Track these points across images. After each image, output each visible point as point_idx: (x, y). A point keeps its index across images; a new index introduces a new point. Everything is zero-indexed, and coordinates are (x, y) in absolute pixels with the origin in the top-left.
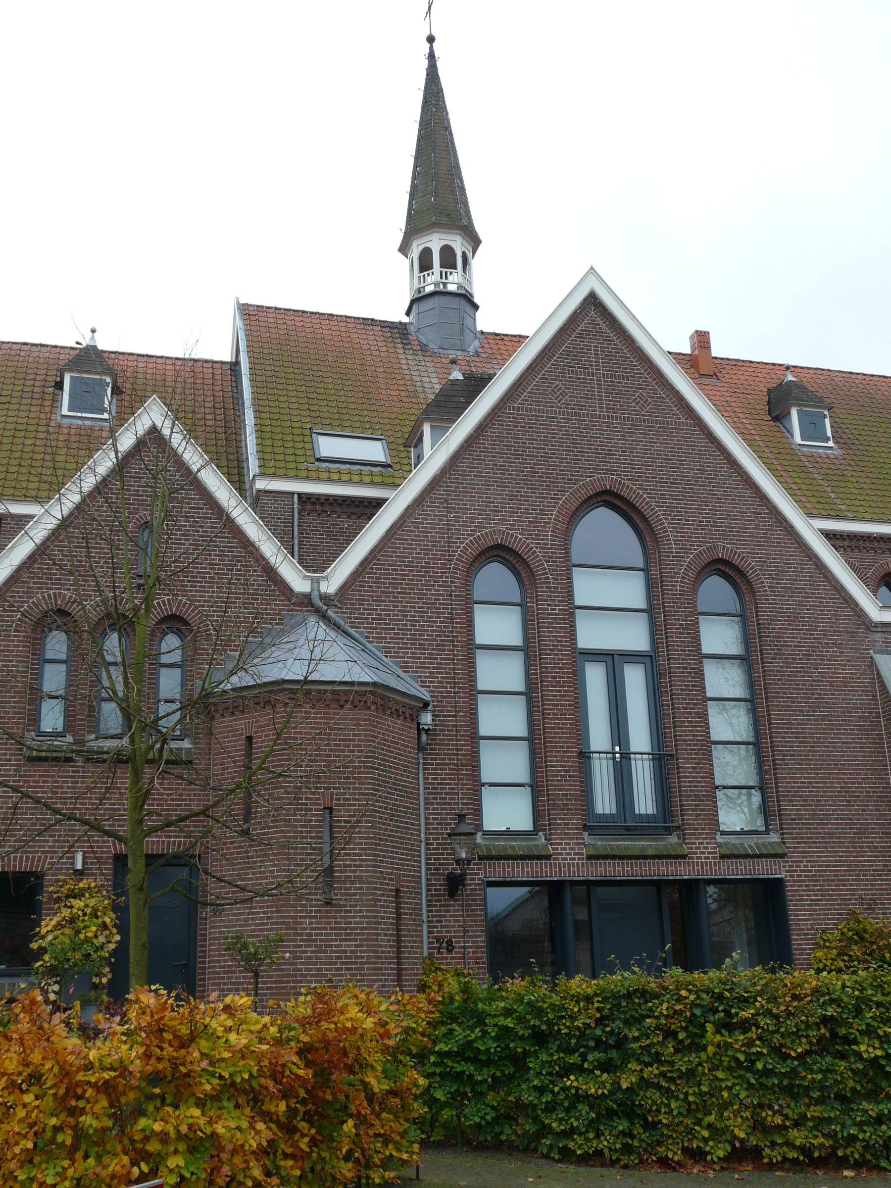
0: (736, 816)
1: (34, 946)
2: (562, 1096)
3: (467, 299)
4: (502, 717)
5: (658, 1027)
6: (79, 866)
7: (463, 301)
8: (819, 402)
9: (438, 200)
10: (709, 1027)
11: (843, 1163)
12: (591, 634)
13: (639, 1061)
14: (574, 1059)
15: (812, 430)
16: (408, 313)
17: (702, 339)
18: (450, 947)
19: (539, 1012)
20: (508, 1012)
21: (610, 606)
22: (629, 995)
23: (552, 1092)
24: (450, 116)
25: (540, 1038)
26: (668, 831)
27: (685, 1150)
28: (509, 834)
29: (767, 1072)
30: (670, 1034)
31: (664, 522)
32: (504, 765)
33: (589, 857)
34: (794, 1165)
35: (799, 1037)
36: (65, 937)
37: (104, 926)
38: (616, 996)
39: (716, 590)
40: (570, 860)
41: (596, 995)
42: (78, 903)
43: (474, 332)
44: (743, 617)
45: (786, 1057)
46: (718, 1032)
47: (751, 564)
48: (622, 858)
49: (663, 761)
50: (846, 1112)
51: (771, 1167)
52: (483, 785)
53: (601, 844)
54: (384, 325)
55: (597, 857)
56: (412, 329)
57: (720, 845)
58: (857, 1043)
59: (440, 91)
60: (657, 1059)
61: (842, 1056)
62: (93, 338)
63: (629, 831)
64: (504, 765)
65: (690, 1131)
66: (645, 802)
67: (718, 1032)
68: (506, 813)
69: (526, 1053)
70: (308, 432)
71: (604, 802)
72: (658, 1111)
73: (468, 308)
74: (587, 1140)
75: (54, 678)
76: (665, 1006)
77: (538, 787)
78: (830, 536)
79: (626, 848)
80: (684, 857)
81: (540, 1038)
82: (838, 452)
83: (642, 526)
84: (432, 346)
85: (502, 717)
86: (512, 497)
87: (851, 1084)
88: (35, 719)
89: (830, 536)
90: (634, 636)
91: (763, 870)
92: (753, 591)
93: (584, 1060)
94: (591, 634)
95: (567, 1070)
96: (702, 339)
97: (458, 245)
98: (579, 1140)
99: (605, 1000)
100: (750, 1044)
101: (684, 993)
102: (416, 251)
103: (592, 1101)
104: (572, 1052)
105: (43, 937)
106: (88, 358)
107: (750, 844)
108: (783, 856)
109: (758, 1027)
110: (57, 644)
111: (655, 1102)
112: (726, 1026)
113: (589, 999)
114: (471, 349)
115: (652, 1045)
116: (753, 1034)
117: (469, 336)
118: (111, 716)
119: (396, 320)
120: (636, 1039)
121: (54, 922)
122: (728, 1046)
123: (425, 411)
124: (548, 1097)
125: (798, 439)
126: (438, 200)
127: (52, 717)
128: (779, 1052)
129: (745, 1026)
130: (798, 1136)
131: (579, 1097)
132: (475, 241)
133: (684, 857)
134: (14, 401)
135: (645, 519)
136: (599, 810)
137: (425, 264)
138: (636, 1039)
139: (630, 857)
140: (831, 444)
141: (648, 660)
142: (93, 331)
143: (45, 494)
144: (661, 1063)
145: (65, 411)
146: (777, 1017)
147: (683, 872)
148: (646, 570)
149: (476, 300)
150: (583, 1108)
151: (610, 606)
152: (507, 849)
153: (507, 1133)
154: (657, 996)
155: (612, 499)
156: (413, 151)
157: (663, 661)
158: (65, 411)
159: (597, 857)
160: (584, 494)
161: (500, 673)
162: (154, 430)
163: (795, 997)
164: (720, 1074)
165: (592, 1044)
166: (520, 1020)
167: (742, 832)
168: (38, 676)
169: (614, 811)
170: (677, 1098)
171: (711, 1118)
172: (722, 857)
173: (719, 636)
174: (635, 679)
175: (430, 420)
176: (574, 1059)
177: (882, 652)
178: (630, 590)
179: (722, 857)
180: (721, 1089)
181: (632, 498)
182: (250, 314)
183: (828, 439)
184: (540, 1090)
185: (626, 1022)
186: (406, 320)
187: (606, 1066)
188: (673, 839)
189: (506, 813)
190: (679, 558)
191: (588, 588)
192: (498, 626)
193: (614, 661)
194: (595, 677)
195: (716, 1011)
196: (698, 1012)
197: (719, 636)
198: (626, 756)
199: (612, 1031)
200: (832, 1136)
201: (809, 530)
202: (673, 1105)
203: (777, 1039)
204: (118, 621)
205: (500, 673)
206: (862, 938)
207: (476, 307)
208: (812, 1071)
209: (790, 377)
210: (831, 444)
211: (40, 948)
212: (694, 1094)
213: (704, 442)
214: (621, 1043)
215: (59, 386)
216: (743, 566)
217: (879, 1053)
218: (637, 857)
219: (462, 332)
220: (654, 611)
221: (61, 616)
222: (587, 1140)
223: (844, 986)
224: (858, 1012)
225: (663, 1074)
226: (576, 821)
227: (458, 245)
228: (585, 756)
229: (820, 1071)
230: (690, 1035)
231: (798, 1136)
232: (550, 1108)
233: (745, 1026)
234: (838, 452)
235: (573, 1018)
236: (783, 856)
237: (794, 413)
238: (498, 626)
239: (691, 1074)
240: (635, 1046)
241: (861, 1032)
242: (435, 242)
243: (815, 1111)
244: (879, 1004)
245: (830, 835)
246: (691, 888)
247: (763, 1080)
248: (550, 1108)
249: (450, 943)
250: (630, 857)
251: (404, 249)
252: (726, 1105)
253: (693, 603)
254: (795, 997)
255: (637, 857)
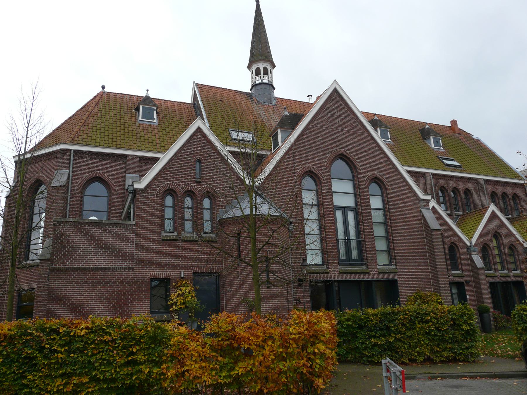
0: (382, 259)
1: (169, 303)
2: (370, 345)
3: (271, 86)
4: (312, 227)
5: (399, 323)
6: (182, 276)
7: (262, 85)
8: (386, 127)
9: (260, 52)
10: (416, 322)
11: (459, 361)
12: (338, 201)
13: (394, 333)
14: (373, 333)
15: (437, 143)
16: (251, 90)
17: (454, 122)
18: (300, 302)
19: (360, 319)
20: (348, 320)
21: (343, 193)
22: (389, 314)
23: (366, 344)
24: (265, 22)
25: (361, 327)
26: (362, 265)
27: (409, 359)
28: (315, 265)
29: (435, 335)
30: (403, 325)
31: (359, 165)
32: (312, 242)
33: (340, 273)
34: (442, 362)
35: (445, 324)
36: (180, 300)
37: (192, 296)
38: (385, 314)
39: (374, 188)
40: (335, 274)
41: (378, 314)
42: (183, 289)
43: (274, 97)
44: (382, 196)
45: (440, 331)
46: (419, 324)
47: (385, 179)
48: (350, 273)
49: (360, 243)
50: (459, 346)
51: (436, 363)
52: (307, 249)
53: (343, 269)
54: (244, 93)
55: (343, 273)
56: (253, 95)
57: (378, 269)
58: (462, 326)
59: (261, 13)
60: (400, 332)
61: (457, 330)
62: (147, 93)
63: (351, 265)
64: (312, 242)
65: (411, 354)
66: (355, 255)
67: (419, 324)
68: (314, 258)
69: (357, 332)
70: (227, 130)
71: (343, 256)
72: (401, 348)
73: (272, 90)
74: (378, 358)
75: (169, 213)
76: (401, 316)
77: (324, 251)
78: (409, 172)
79: (351, 270)
80: (368, 273)
81: (361, 327)
82: (392, 143)
83: (352, 166)
84: (261, 101)
85: (312, 227)
86: (313, 155)
87: (460, 338)
88: (163, 227)
89: (409, 172)
90: (349, 201)
91: (391, 277)
92: (386, 188)
93: (376, 333)
94: (338, 201)
95: (370, 338)
96: (454, 122)
97: (269, 67)
98: (376, 358)
99: (382, 315)
100: (429, 327)
101: (407, 312)
102: (254, 68)
103: (379, 346)
104: (371, 331)
105: (172, 300)
106: (147, 100)
107: (387, 268)
108: (396, 273)
109: (432, 322)
110: (169, 201)
111: (399, 346)
112: (422, 321)
113: (376, 315)
114: (274, 103)
115: (398, 328)
116: (430, 324)
117: (273, 99)
118: (188, 226)
119: (248, 92)
120: (393, 327)
121: (176, 295)
122: (423, 328)
123: (278, 125)
124: (364, 346)
125: (433, 146)
126: (260, 52)
127: (169, 225)
128: (438, 329)
129: (427, 322)
130: (445, 354)
131: (375, 345)
132: (274, 66)
133: (368, 273)
134: (122, 114)
135: (353, 163)
136: (353, 258)
137: (258, 73)
138: (393, 327)
139: (352, 273)
140: (390, 140)
141: (354, 210)
142: (147, 91)
143: (163, 151)
144: (401, 334)
145: (140, 119)
146: (437, 319)
147: (368, 278)
148: (353, 180)
149: (274, 86)
150: (377, 348)
151: (343, 193)
152: (314, 271)
153: (350, 357)
154: (397, 313)
155: (343, 157)
156: (252, 34)
157: (360, 210)
158: (140, 119)
159: (343, 273)
160: (335, 155)
161: (311, 214)
162: (199, 129)
163: (442, 313)
164: (420, 337)
165: (378, 329)
166: (354, 322)
167: (384, 265)
168: (163, 212)
169: (345, 258)
170: (406, 344)
171: (418, 349)
172: (380, 273)
173: (376, 202)
174: (351, 216)
175: (280, 128)
176: (373, 333)
177: (424, 208)
178: (348, 187)
179: (380, 273)
180: (421, 341)
181: (349, 156)
182: (200, 87)
183: (389, 139)
184: (362, 343)
185: (389, 322)
186: (250, 92)
187: (383, 335)
188: (364, 267)
189: (314, 258)
190: (364, 177)
191: (337, 186)
192: (309, 197)
193: (344, 209)
194: (339, 215)
195: (418, 317)
196: (412, 318)
197: (376, 202)
198: (349, 240)
199: (385, 325)
200: (455, 353)
201: (403, 170)
202: (406, 346)
203: (437, 325)
204: (190, 193)
205: (311, 214)
206: (421, 298)
207: (274, 89)
208: (449, 334)
209: (376, 118)
210: (390, 140)
211: (171, 304)
212: (412, 342)
213: (370, 139)
214: (388, 328)
215: (138, 109)
216: (383, 180)
217: (469, 328)
218: (354, 273)
219: (271, 98)
220: (357, 193)
221: (171, 192)
222: (378, 358)
223: (456, 309)
224: (462, 316)
225: (402, 337)
226: (336, 261)
227: (269, 67)
228: (337, 240)
229: (451, 334)
230: (410, 325)
231: (445, 354)
232: (365, 349)
233: (427, 322)
234: (392, 143)
235: (372, 321)
236: (396, 273)
237: (432, 138)
238: (309, 197)
239: (411, 337)
240: (393, 329)
241: (463, 322)
242: (261, 66)
243: (449, 346)
244: (468, 314)
245: (410, 266)
246: (369, 283)
247: (433, 337)
248: (365, 349)
249: (299, 301)
250: (352, 273)
251: (249, 67)
252: (422, 346)
253: (368, 191)
254: (442, 313)
255: (354, 273)
